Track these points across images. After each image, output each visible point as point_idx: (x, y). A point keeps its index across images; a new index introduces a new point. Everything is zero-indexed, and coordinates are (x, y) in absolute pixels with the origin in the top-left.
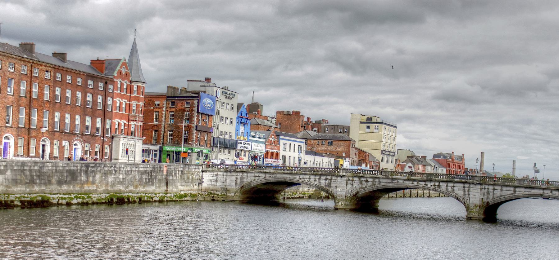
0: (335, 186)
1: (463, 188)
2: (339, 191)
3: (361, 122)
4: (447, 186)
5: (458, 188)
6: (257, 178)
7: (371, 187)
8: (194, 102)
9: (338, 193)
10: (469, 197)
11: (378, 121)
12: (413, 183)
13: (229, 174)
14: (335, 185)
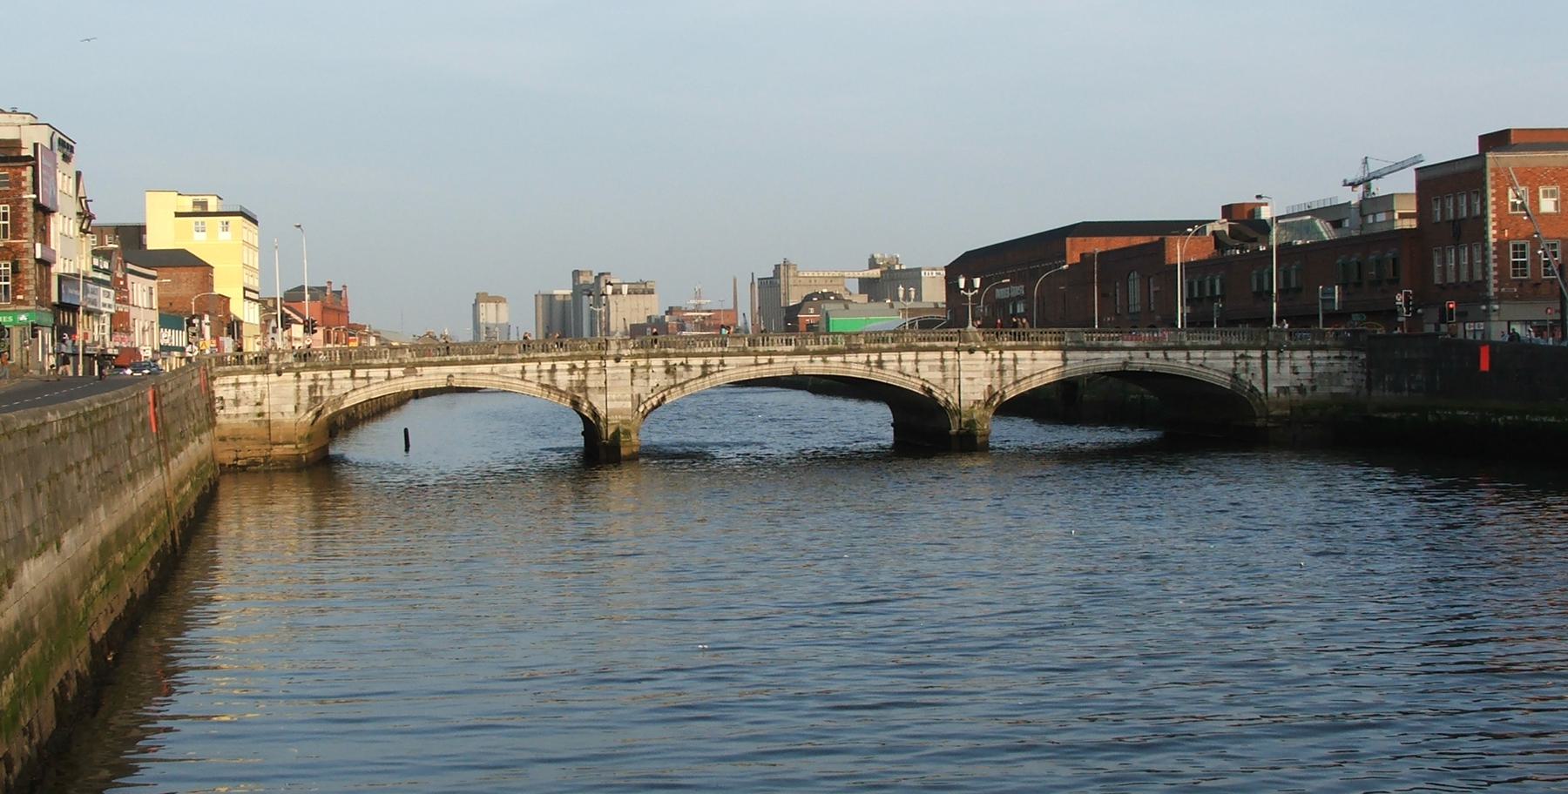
8: (24, 174)
12: (811, 361)
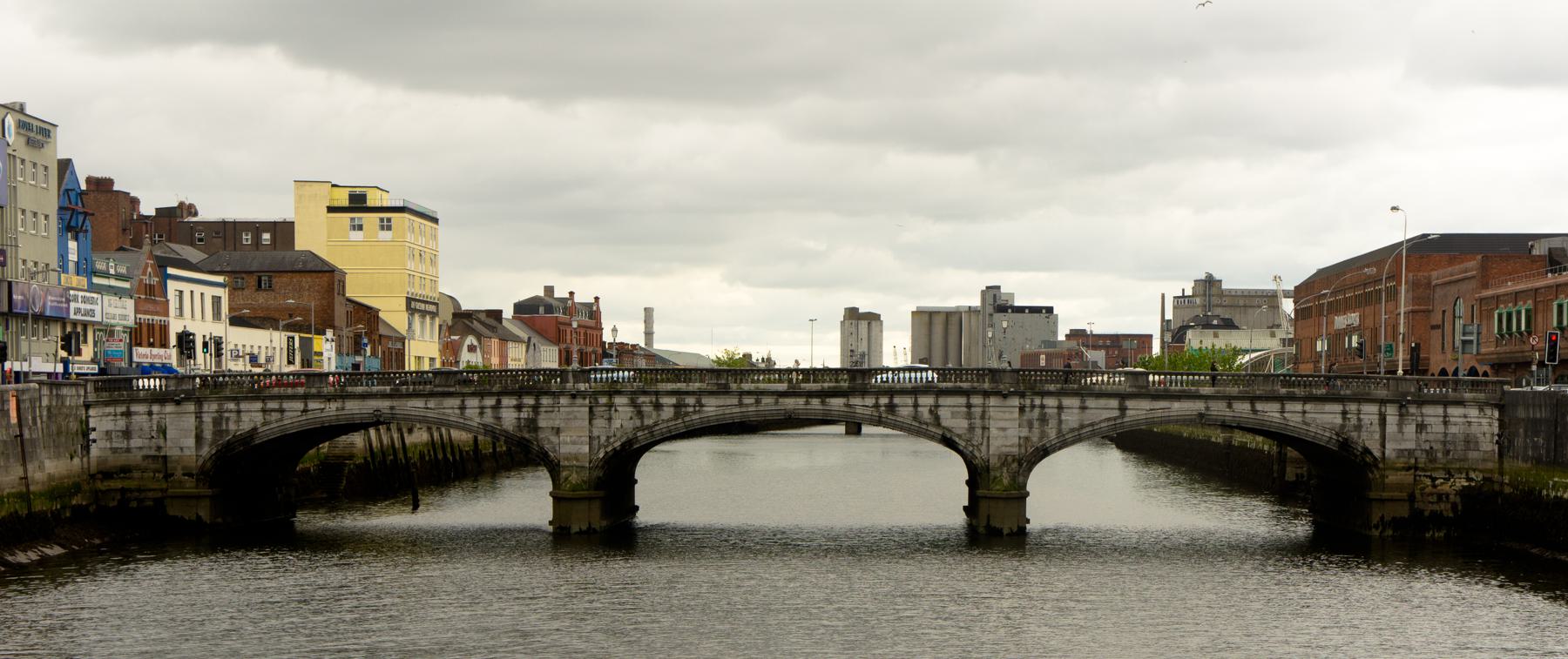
0: (553, 428)
1: (965, 409)
2: (566, 443)
3: (331, 209)
4: (916, 406)
5: (951, 408)
6: (275, 416)
7: (673, 423)
9: (565, 450)
10: (986, 434)
11: (385, 204)
13: (169, 408)
14: (551, 424)
